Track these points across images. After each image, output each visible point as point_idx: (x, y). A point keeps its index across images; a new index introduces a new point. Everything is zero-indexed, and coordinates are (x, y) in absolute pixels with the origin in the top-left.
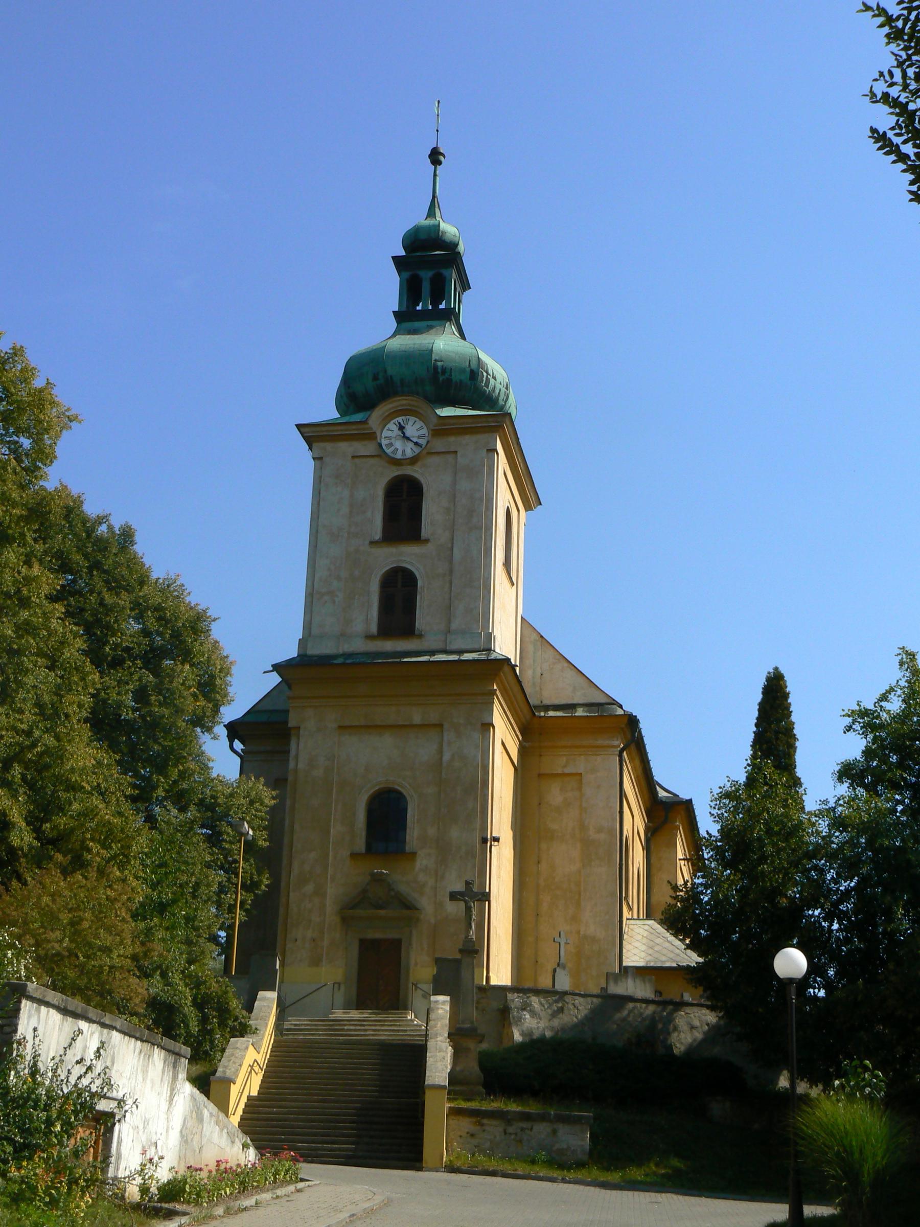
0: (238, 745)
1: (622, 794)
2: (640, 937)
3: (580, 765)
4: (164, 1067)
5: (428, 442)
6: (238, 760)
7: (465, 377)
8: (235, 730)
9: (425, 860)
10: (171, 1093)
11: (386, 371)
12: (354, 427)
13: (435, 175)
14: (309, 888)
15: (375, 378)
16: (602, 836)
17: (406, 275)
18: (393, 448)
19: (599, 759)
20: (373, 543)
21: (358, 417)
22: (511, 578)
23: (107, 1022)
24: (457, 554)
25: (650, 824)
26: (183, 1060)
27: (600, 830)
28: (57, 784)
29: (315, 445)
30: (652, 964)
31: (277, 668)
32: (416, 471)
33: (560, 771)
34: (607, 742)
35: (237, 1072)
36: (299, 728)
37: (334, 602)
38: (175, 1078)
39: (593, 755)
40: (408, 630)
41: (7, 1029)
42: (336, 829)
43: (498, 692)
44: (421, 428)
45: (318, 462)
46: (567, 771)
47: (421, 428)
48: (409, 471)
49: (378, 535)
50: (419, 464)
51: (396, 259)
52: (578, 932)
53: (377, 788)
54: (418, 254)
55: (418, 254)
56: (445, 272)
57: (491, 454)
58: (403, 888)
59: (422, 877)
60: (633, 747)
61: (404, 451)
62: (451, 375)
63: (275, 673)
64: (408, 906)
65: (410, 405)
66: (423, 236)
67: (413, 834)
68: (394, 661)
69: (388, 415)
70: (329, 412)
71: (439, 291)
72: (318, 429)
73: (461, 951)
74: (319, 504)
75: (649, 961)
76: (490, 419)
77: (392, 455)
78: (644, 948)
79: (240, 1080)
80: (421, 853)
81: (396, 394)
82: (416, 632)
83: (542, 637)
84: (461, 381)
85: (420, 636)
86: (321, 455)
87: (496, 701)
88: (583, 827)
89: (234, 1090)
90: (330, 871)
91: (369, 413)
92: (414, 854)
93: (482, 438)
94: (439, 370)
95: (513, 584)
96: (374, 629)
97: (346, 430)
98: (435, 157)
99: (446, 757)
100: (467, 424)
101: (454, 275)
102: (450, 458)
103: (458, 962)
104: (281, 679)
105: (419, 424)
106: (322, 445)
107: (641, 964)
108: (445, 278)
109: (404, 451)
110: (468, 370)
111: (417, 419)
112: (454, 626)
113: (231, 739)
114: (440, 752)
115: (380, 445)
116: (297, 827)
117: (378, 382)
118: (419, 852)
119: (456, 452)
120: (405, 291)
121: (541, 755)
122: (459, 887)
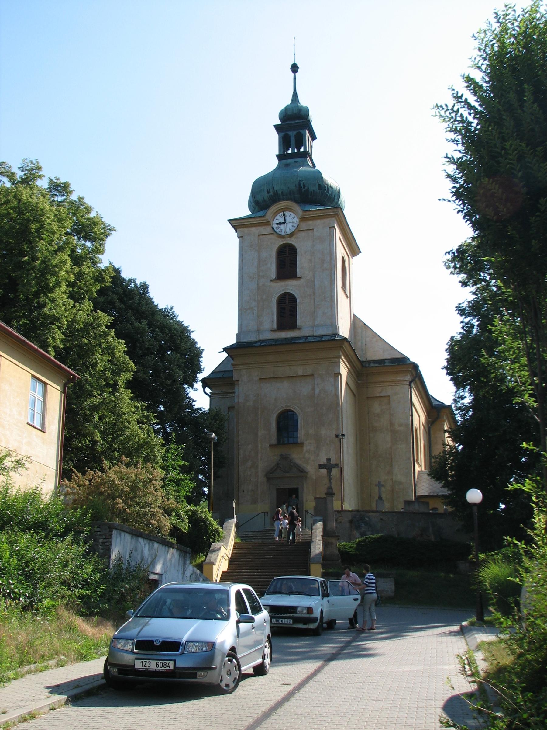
0: (208, 390)
1: (412, 404)
2: (425, 480)
3: (389, 391)
4: (179, 559)
5: (298, 225)
6: (208, 398)
7: (316, 188)
8: (205, 383)
9: (309, 446)
10: (184, 570)
11: (273, 188)
12: (258, 219)
13: (295, 79)
14: (249, 464)
15: (268, 192)
16: (402, 428)
17: (282, 134)
18: (279, 229)
19: (399, 387)
20: (271, 280)
21: (260, 214)
22: (346, 295)
23: (152, 539)
24: (317, 284)
25: (430, 419)
26: (188, 554)
27: (400, 425)
28: (84, 549)
29: (238, 230)
30: (432, 494)
31: (225, 350)
32: (292, 241)
33: (378, 395)
34: (402, 378)
35: (216, 559)
36: (238, 381)
37: (253, 313)
38: (185, 563)
39: (395, 385)
40: (293, 326)
41: (108, 544)
42: (261, 433)
43: (342, 357)
44: (294, 217)
45: (241, 239)
46: (382, 394)
47: (294, 217)
48: (289, 241)
49: (274, 277)
50: (294, 237)
51: (276, 127)
52: (392, 479)
53: (281, 410)
54: (287, 123)
55: (287, 123)
56: (302, 131)
57: (332, 229)
58: (298, 461)
59: (307, 455)
60: (417, 379)
61: (285, 230)
62: (308, 188)
63: (224, 352)
64: (302, 471)
65: (287, 206)
66: (290, 113)
67: (301, 433)
68: (288, 342)
69: (276, 212)
70: (245, 212)
71: (300, 142)
72: (239, 221)
73: (326, 494)
74: (242, 262)
75: (431, 493)
76: (330, 211)
77: (280, 233)
78: (427, 486)
79: (217, 563)
80: (306, 443)
81: (280, 200)
82: (298, 327)
83: (365, 324)
84: (314, 191)
85: (300, 329)
86: (242, 235)
87: (341, 361)
88: (392, 424)
89: (215, 568)
90: (259, 455)
91: (266, 211)
92: (302, 444)
93: (327, 221)
94: (302, 186)
95: (347, 297)
96: (275, 326)
97: (255, 221)
98: (294, 68)
99: (317, 391)
100: (318, 214)
101: (307, 133)
102: (310, 232)
103: (325, 498)
104: (227, 355)
105: (293, 215)
106: (241, 229)
107: (426, 494)
108: (302, 135)
109: (285, 230)
110: (317, 184)
111: (292, 213)
112: (317, 323)
113: (204, 387)
114: (313, 389)
115: (273, 228)
116: (241, 432)
117: (270, 194)
118: (305, 443)
119: (313, 229)
120: (282, 143)
121: (367, 387)
122: (324, 461)
